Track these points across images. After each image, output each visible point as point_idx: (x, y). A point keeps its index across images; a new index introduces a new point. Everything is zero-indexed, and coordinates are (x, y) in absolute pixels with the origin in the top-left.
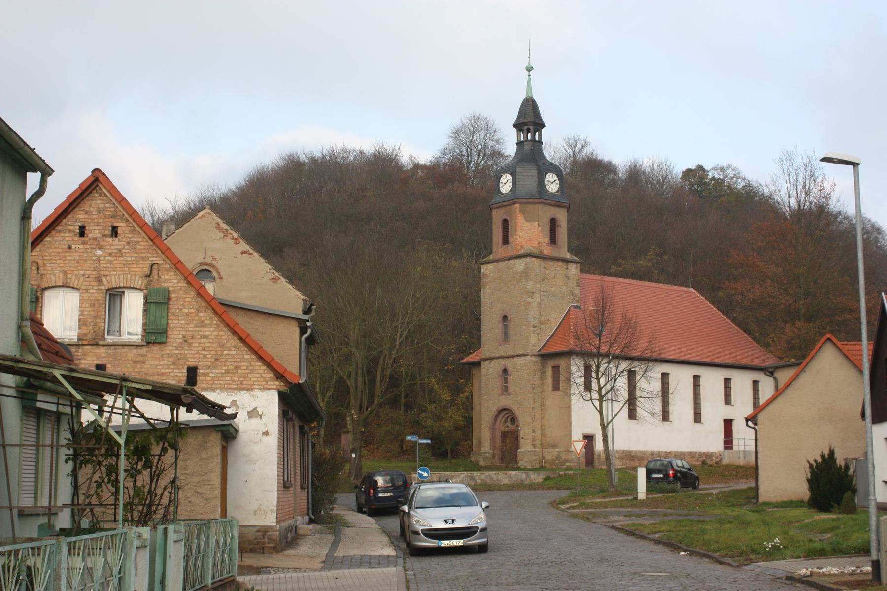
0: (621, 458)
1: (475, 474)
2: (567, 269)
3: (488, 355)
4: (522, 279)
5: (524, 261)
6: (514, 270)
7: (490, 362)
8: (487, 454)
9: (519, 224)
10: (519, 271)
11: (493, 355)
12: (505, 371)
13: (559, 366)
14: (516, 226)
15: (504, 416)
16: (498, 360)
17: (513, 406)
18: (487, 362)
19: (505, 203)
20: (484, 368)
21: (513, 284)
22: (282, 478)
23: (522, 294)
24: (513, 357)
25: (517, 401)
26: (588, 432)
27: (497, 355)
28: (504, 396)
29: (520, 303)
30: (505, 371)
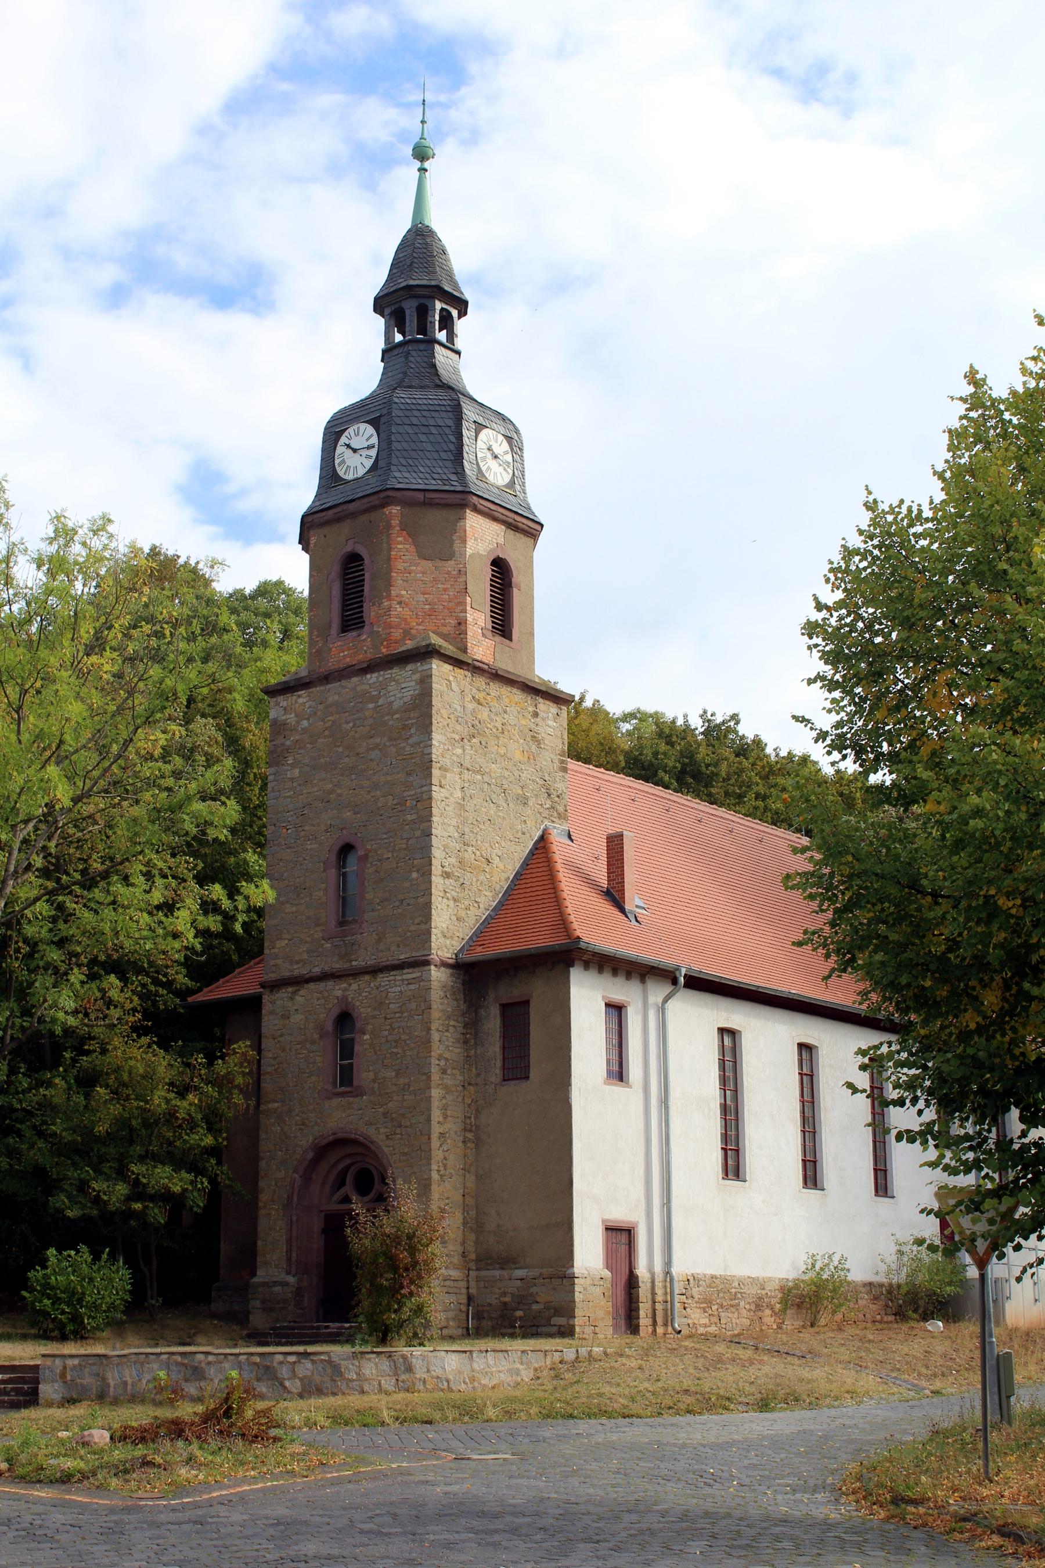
0: (706, 1303)
1: (279, 1358)
2: (536, 715)
3: (286, 971)
4: (408, 727)
5: (414, 672)
6: (381, 702)
7: (294, 993)
8: (277, 1289)
9: (400, 565)
10: (397, 704)
11: (299, 970)
12: (345, 1019)
13: (527, 1002)
14: (389, 571)
15: (342, 1158)
16: (321, 985)
17: (371, 1131)
18: (283, 994)
19: (352, 507)
20: (272, 1012)
21: (377, 746)
22: (463, 1284)
23: (409, 774)
24: (374, 971)
25: (385, 1114)
26: (620, 1215)
27: (317, 970)
28: (336, 1101)
29: (402, 803)
30: (345, 1019)
